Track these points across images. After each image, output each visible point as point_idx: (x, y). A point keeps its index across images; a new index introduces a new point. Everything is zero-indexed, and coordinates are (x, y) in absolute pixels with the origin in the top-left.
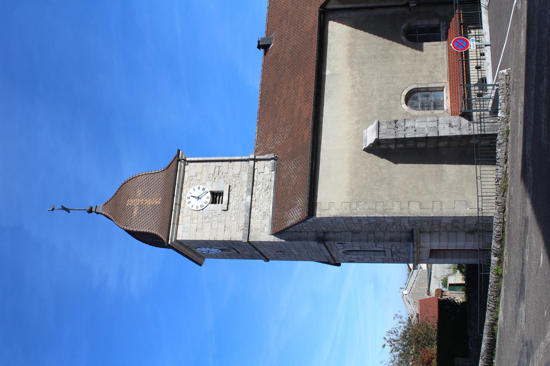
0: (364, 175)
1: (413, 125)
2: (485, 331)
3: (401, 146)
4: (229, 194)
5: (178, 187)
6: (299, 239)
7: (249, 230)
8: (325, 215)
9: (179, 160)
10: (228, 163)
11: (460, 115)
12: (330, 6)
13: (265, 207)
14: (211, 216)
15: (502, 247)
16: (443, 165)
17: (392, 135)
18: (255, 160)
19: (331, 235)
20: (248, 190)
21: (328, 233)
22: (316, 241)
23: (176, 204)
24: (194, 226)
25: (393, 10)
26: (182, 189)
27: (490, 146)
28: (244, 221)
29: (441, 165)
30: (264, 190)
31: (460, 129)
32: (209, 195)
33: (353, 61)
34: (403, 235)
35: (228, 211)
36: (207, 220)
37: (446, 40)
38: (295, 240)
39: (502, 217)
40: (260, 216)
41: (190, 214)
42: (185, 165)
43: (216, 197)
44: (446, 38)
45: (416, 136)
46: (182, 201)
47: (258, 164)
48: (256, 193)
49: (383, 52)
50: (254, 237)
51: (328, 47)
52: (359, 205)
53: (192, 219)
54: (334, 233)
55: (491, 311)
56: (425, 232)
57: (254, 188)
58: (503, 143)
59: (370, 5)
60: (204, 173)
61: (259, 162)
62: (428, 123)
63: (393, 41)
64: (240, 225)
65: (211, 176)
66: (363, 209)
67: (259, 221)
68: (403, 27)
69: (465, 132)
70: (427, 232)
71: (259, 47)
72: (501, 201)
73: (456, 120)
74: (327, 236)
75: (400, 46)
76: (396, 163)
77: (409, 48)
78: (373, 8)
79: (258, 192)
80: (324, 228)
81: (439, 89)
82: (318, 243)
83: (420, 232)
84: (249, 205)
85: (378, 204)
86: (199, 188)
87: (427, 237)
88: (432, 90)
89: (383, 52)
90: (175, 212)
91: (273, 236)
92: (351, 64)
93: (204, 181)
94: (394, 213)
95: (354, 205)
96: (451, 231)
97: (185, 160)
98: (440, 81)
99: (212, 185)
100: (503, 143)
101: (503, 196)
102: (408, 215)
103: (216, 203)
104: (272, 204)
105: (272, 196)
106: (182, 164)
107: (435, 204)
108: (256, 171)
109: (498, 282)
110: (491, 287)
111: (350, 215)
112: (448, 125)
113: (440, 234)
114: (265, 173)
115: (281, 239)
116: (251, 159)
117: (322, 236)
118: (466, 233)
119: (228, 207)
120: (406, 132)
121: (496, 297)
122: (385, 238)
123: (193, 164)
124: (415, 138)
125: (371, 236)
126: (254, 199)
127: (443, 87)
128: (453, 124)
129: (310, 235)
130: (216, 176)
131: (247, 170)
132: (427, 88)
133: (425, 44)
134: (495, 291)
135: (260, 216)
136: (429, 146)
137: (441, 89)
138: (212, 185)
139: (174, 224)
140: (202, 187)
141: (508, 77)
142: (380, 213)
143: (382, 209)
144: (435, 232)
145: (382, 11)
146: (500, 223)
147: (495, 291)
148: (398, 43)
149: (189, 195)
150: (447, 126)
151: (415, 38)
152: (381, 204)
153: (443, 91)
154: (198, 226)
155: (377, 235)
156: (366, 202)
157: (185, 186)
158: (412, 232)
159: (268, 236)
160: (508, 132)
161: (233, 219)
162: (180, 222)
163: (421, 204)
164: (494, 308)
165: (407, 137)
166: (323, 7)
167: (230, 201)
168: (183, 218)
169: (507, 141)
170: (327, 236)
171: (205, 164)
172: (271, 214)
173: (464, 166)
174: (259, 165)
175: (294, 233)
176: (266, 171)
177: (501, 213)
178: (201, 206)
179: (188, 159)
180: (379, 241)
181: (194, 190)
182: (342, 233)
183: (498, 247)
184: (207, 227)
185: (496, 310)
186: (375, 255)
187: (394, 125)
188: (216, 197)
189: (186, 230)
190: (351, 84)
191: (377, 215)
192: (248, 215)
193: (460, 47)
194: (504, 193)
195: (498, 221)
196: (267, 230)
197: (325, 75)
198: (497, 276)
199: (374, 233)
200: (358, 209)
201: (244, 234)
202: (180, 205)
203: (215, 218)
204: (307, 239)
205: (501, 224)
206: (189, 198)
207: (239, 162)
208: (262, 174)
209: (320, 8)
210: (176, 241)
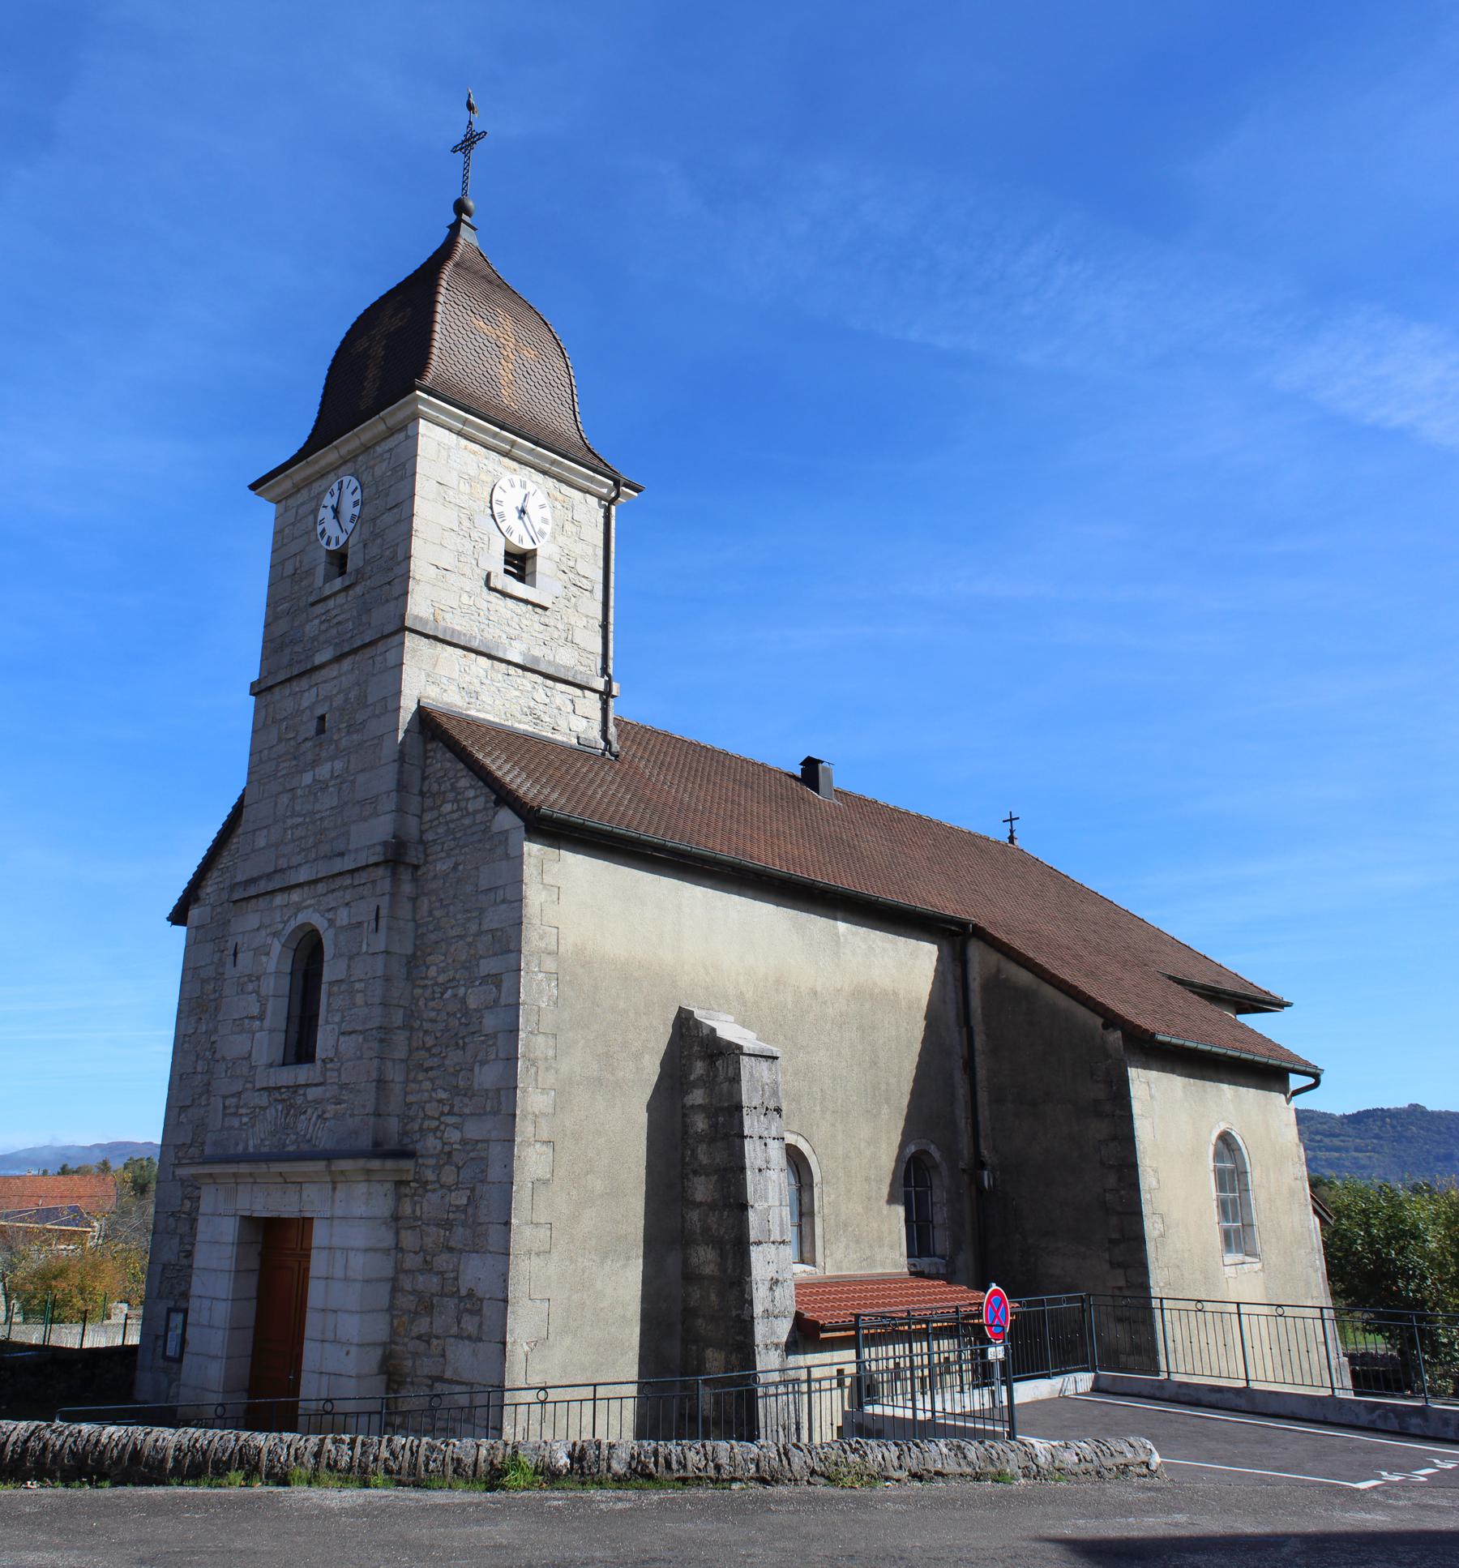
0: (622, 1005)
1: (772, 1166)
2: (138, 1431)
3: (700, 1124)
4: (526, 602)
5: (553, 462)
6: (401, 787)
7: (436, 638)
8: (529, 871)
9: (617, 484)
10: (600, 618)
11: (797, 1313)
12: (976, 952)
13: (489, 701)
14: (475, 535)
15: (620, 1481)
16: (641, 1261)
17: (750, 1098)
18: (606, 696)
19: (407, 888)
20: (536, 659)
21: (415, 880)
22: (394, 837)
23: (513, 444)
24: (452, 479)
25: (963, 1123)
26: (544, 473)
27: (693, 1418)
28: (458, 628)
29: (641, 1252)
30: (532, 704)
31: (767, 1313)
32: (527, 545)
33: (869, 999)
34: (393, 1125)
35: (485, 589)
36: (466, 523)
37: (912, 1273)
38: (400, 772)
39: (738, 1474)
40: (468, 678)
41: (483, 477)
42: (600, 498)
43: (520, 563)
44: (917, 1274)
45: (748, 1173)
46: (514, 465)
47: (593, 703)
48: (525, 682)
49: (883, 1087)
50: (414, 650)
51: (891, 936)
52: (549, 981)
53: (470, 481)
54: (414, 900)
55: (317, 1455)
56: (398, 1198)
57: (539, 679)
58: (969, 1464)
59: (980, 1060)
60: (580, 544)
61: (599, 705)
62: (777, 1210)
63: (908, 1119)
64: (448, 616)
65: (571, 564)
66: (540, 992)
67: (456, 675)
68: (933, 1149)
69: (760, 1331)
70: (397, 1207)
71: (811, 766)
72: (795, 1467)
73: (786, 1298)
74: (405, 875)
75: (897, 1138)
76: (651, 1107)
77: (893, 1164)
78: (969, 1066)
79: (529, 687)
80: (442, 867)
81: (807, 1248)
82: (385, 844)
83: (399, 1184)
84: (501, 655)
85: (551, 1042)
86: (545, 521)
87: (382, 1206)
88: (806, 1229)
89: (883, 1087)
90: (495, 435)
91: (414, 707)
92: (860, 994)
93: (561, 539)
94: (525, 1091)
95: (550, 965)
96: (395, 1290)
97: (612, 501)
98: (828, 1252)
99: (549, 558)
100: (969, 1464)
101: (813, 1472)
102: (518, 1140)
103: (506, 562)
104: (497, 720)
105: (516, 725)
106: (605, 491)
107: (543, 1233)
108: (578, 692)
109: (461, 1473)
110: (432, 1448)
111: (525, 949)
112: (775, 1276)
113: (387, 1251)
114: (572, 717)
115: (406, 732)
116: (609, 684)
117: (408, 860)
118: (384, 1344)
119: (495, 590)
120: (758, 1142)
121: (388, 1471)
122: (389, 1064)
123: (601, 521)
124: (743, 1169)
125: (398, 1018)
126: (512, 670)
127: (813, 1263)
128: (778, 1291)
129: (413, 823)
130: (572, 576)
131: (582, 669)
132: (812, 1214)
133: (900, 1211)
134: (414, 1466)
135: (468, 678)
136: (694, 1216)
137: (807, 1255)
138: (549, 558)
139: (465, 422)
140: (547, 529)
141: (1145, 1470)
142: (527, 1046)
143: (538, 1053)
144: (397, 1233)
145: (962, 1091)
146: (718, 1467)
147: (414, 1466)
148: (903, 1134)
149: (531, 487)
150: (770, 1272)
151: (913, 1182)
152: (551, 1053)
153: (802, 1262)
154: (451, 492)
155: (400, 1037)
156: (556, 1003)
157: (551, 482)
158: (410, 1155)
159: (416, 693)
160: (999, 1477)
161: (465, 599)
162: (464, 442)
163: (545, 1182)
164: (332, 1467)
165: (747, 1142)
166: (980, 933)
167: (510, 603)
168: (475, 453)
169: (977, 1477)
170: (405, 875)
171: (600, 553)
172: (472, 713)
173: (637, 1330)
174: (591, 704)
175: (418, 772)
176: (575, 721)
177: (753, 1467)
178: (502, 515)
179: (613, 508)
180: (382, 1041)
181: (542, 506)
182: (411, 925)
183: (615, 1466)
184: (449, 517)
185: (324, 1474)
186: (271, 1031)
187: (772, 1106)
188: (520, 563)
189: (444, 453)
190: (819, 989)
191: (522, 1035)
192: (475, 645)
193: (991, 1315)
194: (822, 1475)
195: (724, 1460)
196: (433, 695)
197: (835, 919)
198: (483, 1467)
199: (407, 1026)
200: (541, 976)
201: (426, 622)
202: (506, 454)
203: (469, 545)
204: (400, 810)
205: (712, 1473)
206: (524, 486)
207: (599, 650)
208: (570, 708)
209: (975, 926)
210: (415, 417)
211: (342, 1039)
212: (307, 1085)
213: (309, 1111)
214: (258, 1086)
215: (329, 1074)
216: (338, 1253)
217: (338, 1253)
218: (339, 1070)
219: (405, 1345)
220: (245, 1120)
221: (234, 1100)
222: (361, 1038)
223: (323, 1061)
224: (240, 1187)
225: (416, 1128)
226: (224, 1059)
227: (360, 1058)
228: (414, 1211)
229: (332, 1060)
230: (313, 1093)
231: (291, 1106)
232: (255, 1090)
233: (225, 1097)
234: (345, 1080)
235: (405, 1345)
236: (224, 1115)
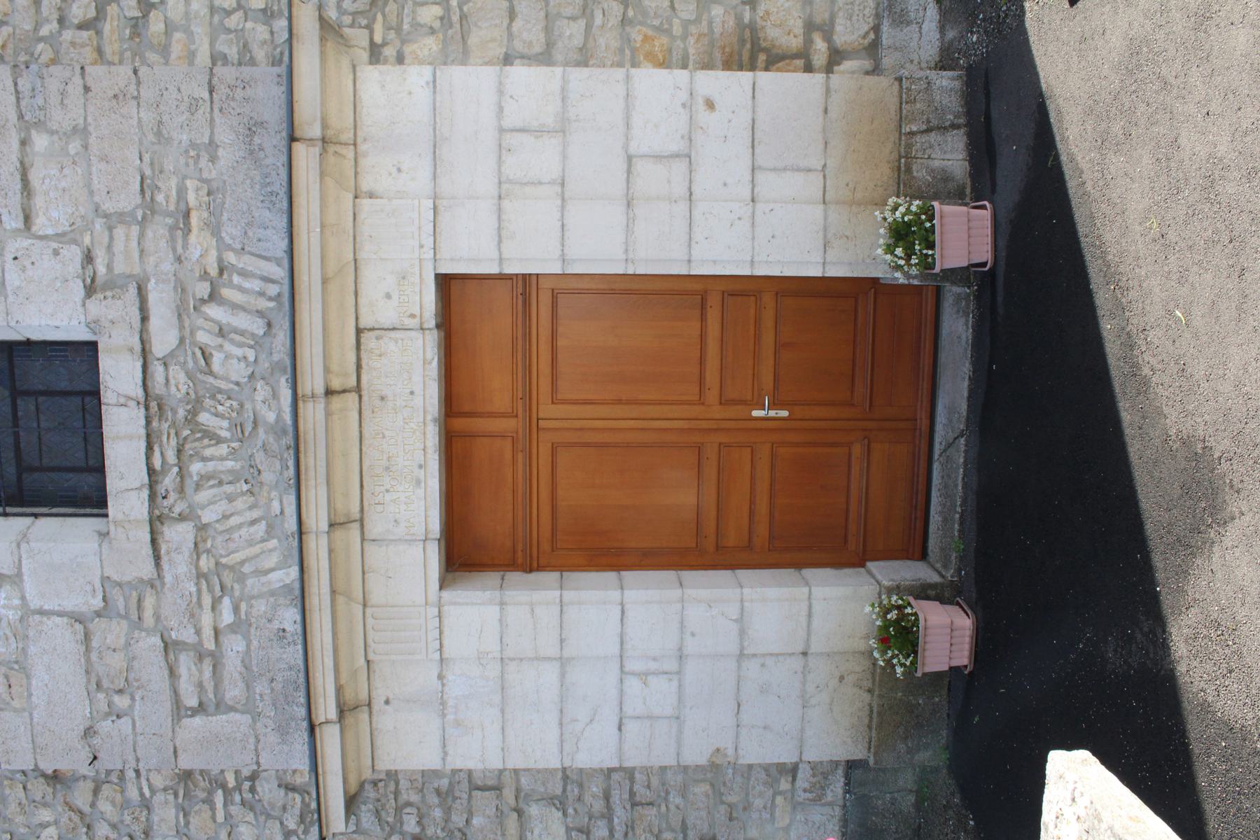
211: (41, 224)
212: (145, 353)
213: (203, 337)
214: (148, 570)
215: (119, 268)
216: (513, 166)
217: (513, 166)
218: (113, 220)
219: (686, 24)
220: (227, 617)
221: (185, 663)
222: (40, 142)
223: (90, 290)
224: (376, 597)
225: (261, 32)
226: (89, 732)
227: (81, 131)
228: (432, 31)
229: (89, 258)
230: (164, 339)
231: (191, 418)
232: (156, 584)
233: (179, 711)
234: (128, 199)
235: (686, 24)
236: (221, 706)
